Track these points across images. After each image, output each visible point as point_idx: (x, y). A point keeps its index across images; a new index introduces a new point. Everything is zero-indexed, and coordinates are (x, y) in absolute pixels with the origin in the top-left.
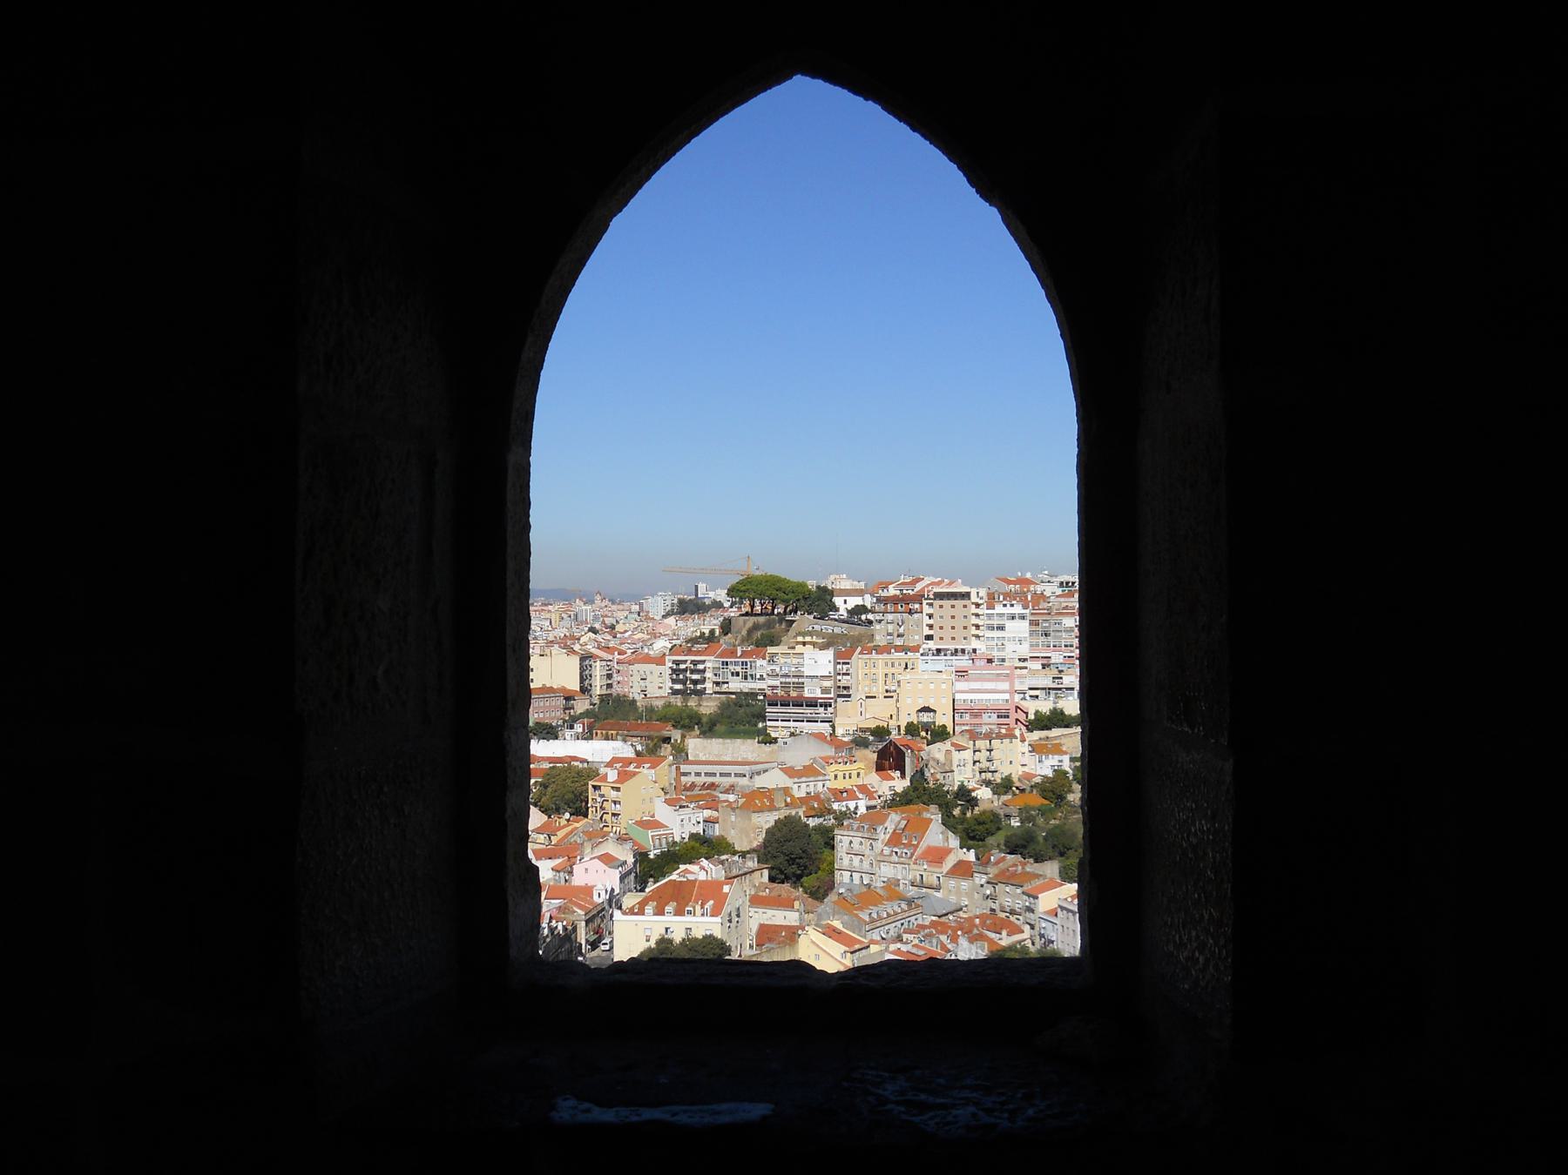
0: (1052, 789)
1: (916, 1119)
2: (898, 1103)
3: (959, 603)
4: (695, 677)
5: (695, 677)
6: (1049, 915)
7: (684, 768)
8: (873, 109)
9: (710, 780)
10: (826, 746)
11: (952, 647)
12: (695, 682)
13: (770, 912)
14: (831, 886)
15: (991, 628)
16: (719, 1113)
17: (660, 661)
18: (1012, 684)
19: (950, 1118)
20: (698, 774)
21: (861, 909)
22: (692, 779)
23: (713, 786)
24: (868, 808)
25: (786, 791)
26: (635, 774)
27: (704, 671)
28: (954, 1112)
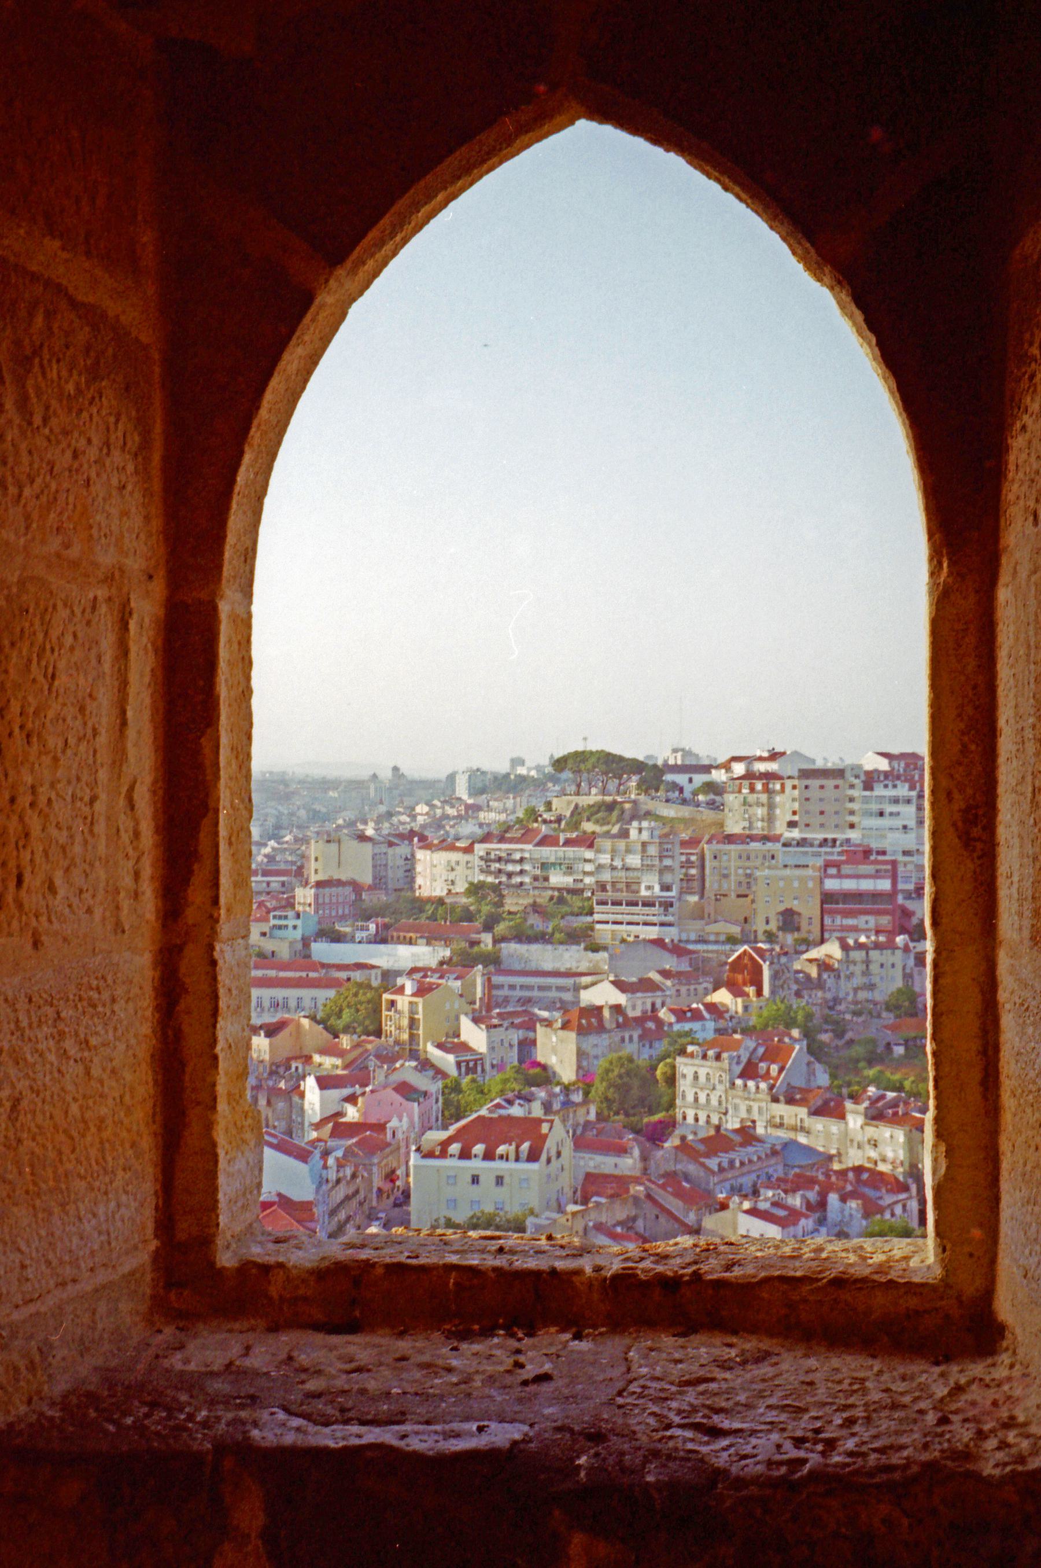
0: (905, 1004)
1: (704, 1449)
2: (681, 1426)
3: (830, 783)
4: (510, 868)
5: (510, 868)
6: (226, 1259)
7: (497, 979)
8: (672, 167)
9: (527, 994)
10: (666, 955)
11: (820, 836)
12: (510, 875)
13: (599, 1159)
14: (669, 1125)
15: (869, 814)
16: (457, 1435)
17: (469, 850)
18: (839, 871)
19: (748, 1450)
20: (512, 987)
21: (708, 1155)
22: (505, 992)
23: (529, 1000)
24: (717, 1031)
25: (617, 1009)
26: (439, 985)
27: (522, 860)
28: (754, 1441)
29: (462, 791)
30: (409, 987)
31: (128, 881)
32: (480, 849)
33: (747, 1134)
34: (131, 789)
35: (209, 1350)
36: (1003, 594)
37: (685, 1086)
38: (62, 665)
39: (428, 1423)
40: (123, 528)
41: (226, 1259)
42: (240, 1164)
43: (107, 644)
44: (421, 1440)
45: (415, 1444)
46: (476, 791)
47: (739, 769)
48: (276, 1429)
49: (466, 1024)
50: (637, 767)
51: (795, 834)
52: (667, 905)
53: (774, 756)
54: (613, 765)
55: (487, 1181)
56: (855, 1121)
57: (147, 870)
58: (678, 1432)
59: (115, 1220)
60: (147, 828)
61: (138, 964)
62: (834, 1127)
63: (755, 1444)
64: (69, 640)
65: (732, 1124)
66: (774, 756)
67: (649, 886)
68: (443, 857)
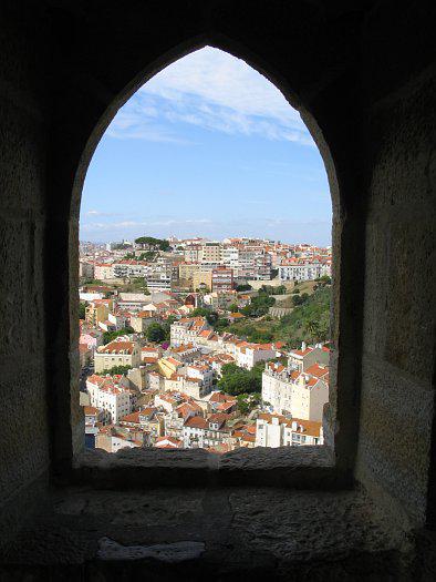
6: (76, 466)
17: (110, 266)
29: (108, 248)
30: (93, 305)
31: (34, 332)
32: (114, 266)
33: (190, 346)
34: (36, 296)
35: (74, 505)
36: (371, 228)
37: (172, 333)
38: (9, 251)
39: (166, 543)
40: (29, 194)
41: (76, 466)
42: (79, 430)
43: (26, 243)
44: (164, 553)
45: (162, 556)
46: (113, 249)
47: (189, 243)
48: (110, 550)
49: (110, 316)
50: (160, 242)
51: (205, 262)
52: (168, 282)
53: (199, 239)
54: (151, 241)
55: (117, 359)
56: (220, 341)
57: (42, 328)
58: (257, 540)
59: (33, 459)
60: (41, 311)
61: (38, 362)
62: (215, 344)
63: (287, 544)
64: (12, 241)
65: (186, 343)
66: (199, 239)
67: (163, 276)
68: (103, 268)
